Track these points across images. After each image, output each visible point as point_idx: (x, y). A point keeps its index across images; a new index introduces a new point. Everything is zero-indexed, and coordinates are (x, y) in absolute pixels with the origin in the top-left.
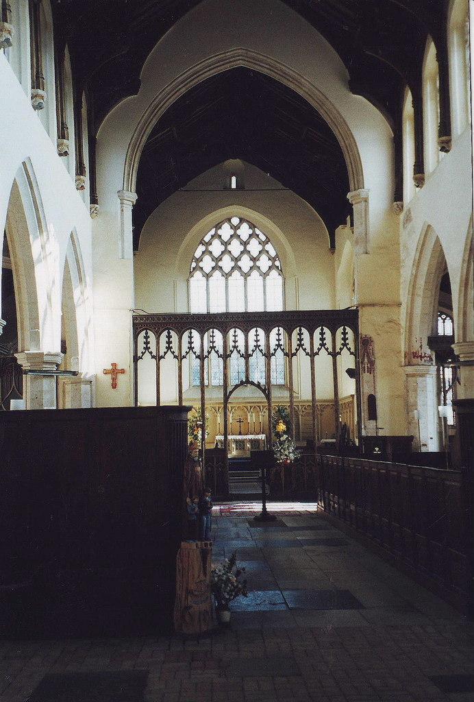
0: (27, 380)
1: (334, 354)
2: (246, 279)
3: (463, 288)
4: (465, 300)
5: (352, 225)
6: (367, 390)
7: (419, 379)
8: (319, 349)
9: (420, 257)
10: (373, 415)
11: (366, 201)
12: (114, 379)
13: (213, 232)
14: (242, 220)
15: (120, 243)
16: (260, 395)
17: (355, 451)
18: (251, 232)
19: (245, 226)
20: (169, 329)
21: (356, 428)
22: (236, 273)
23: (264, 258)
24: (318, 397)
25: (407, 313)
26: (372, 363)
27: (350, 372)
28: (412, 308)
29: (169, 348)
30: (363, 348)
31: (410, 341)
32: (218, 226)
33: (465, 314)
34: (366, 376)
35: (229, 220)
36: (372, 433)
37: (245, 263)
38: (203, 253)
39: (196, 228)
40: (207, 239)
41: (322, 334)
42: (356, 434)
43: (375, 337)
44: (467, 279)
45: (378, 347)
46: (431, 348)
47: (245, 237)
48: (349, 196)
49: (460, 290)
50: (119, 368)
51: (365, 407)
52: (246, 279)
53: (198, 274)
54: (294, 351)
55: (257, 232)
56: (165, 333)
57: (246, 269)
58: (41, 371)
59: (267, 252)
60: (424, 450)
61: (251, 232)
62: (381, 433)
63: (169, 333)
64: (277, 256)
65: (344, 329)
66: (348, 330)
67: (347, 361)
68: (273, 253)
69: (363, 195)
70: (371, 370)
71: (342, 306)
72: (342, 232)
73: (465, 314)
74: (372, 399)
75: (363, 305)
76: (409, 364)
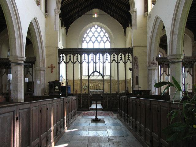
0: (12, 65)
1: (125, 63)
2: (99, 44)
3: (171, 35)
4: (172, 39)
5: (131, 26)
6: (135, 75)
7: (153, 71)
8: (120, 61)
9: (153, 34)
10: (137, 83)
11: (136, 12)
12: (52, 70)
13: (89, 30)
14: (98, 26)
15: (54, 26)
16: (101, 77)
17: (131, 95)
18: (101, 30)
19: (99, 28)
20: (70, 54)
21: (131, 88)
22: (96, 42)
23: (105, 37)
24: (119, 79)
25: (149, 49)
26: (137, 66)
27: (130, 69)
28: (151, 47)
29: (70, 60)
30: (135, 61)
31: (150, 59)
32: (91, 28)
33: (172, 44)
34: (135, 70)
35: (94, 26)
36: (137, 89)
37: (99, 39)
38: (87, 36)
39: (85, 28)
40: (88, 32)
41: (121, 56)
42: (131, 90)
43: (138, 57)
44: (173, 31)
45: (139, 60)
46: (157, 61)
47: (99, 32)
48: (130, 11)
49: (170, 35)
50: (53, 66)
51: (135, 80)
52: (99, 44)
53: (85, 42)
54: (112, 61)
55: (103, 30)
56: (69, 55)
57: (99, 41)
58: (16, 63)
59: (106, 36)
60: (153, 94)
61: (101, 30)
62: (140, 89)
63: (70, 55)
64: (109, 37)
65: (129, 54)
66: (130, 54)
67: (129, 65)
68: (107, 36)
69: (135, 10)
70: (137, 68)
71: (128, 46)
72: (128, 29)
73: (172, 44)
74: (137, 78)
75: (135, 46)
76: (150, 66)
